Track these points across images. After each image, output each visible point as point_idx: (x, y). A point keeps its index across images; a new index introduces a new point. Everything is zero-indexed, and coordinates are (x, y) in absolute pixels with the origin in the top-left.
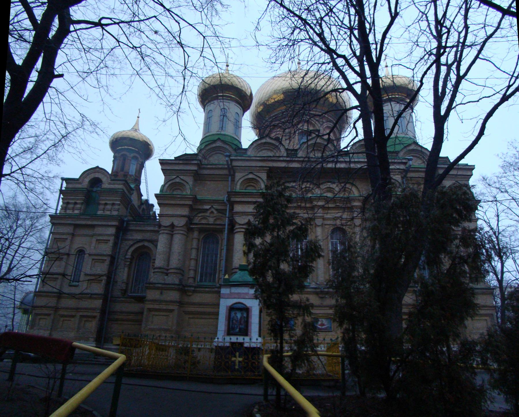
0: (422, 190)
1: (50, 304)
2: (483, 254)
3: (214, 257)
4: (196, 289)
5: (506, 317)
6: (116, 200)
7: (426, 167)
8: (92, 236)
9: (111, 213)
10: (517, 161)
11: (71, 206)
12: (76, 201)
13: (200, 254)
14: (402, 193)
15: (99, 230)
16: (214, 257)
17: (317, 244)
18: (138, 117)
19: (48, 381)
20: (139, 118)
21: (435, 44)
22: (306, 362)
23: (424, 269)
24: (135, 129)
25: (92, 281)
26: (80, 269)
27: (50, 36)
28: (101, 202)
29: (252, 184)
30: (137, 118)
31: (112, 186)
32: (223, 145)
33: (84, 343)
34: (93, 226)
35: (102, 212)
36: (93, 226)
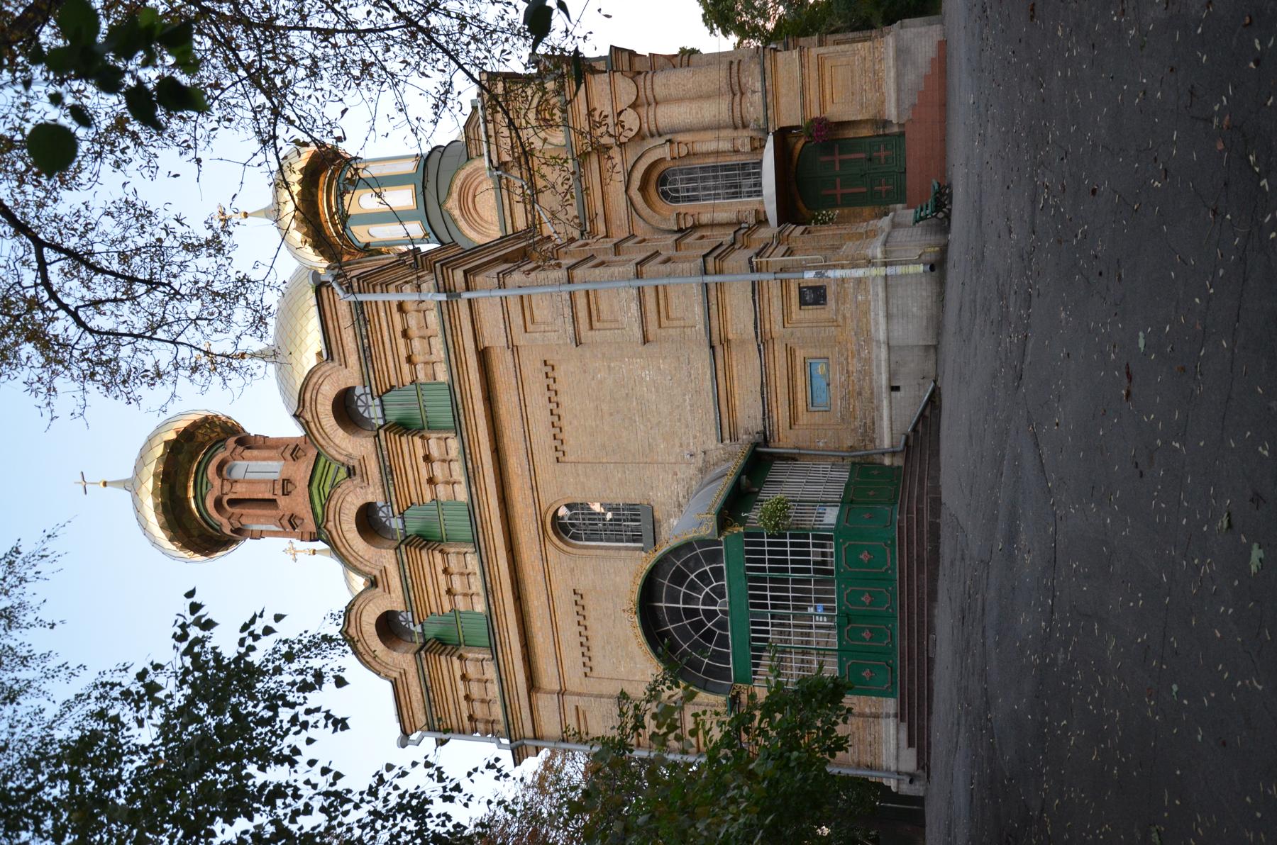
0: (68, 835)
1: (608, 80)
2: (224, 765)
3: (759, 837)
4: (883, 346)
5: (882, 9)
6: (433, 565)
7: (48, 267)
8: (514, 348)
9: (478, 594)
10: (2, 707)
11: (479, 710)
12: (443, 592)
13: (877, 315)
14: (199, 536)
15: (493, 336)
16: (759, 837)
17: (536, 779)
18: (105, 484)
19: (141, 277)
20: (107, 480)
21: (127, 302)
22: (256, 805)
23: (447, 42)
24: (131, 485)
25: (594, 318)
26: (452, 289)
27: (1254, 569)
28: (447, 608)
29: (475, 183)
30: (108, 488)
31: (353, 359)
32: (455, 195)
33: (881, 427)
34: (483, 356)
35: (472, 579)
36: (483, 356)
